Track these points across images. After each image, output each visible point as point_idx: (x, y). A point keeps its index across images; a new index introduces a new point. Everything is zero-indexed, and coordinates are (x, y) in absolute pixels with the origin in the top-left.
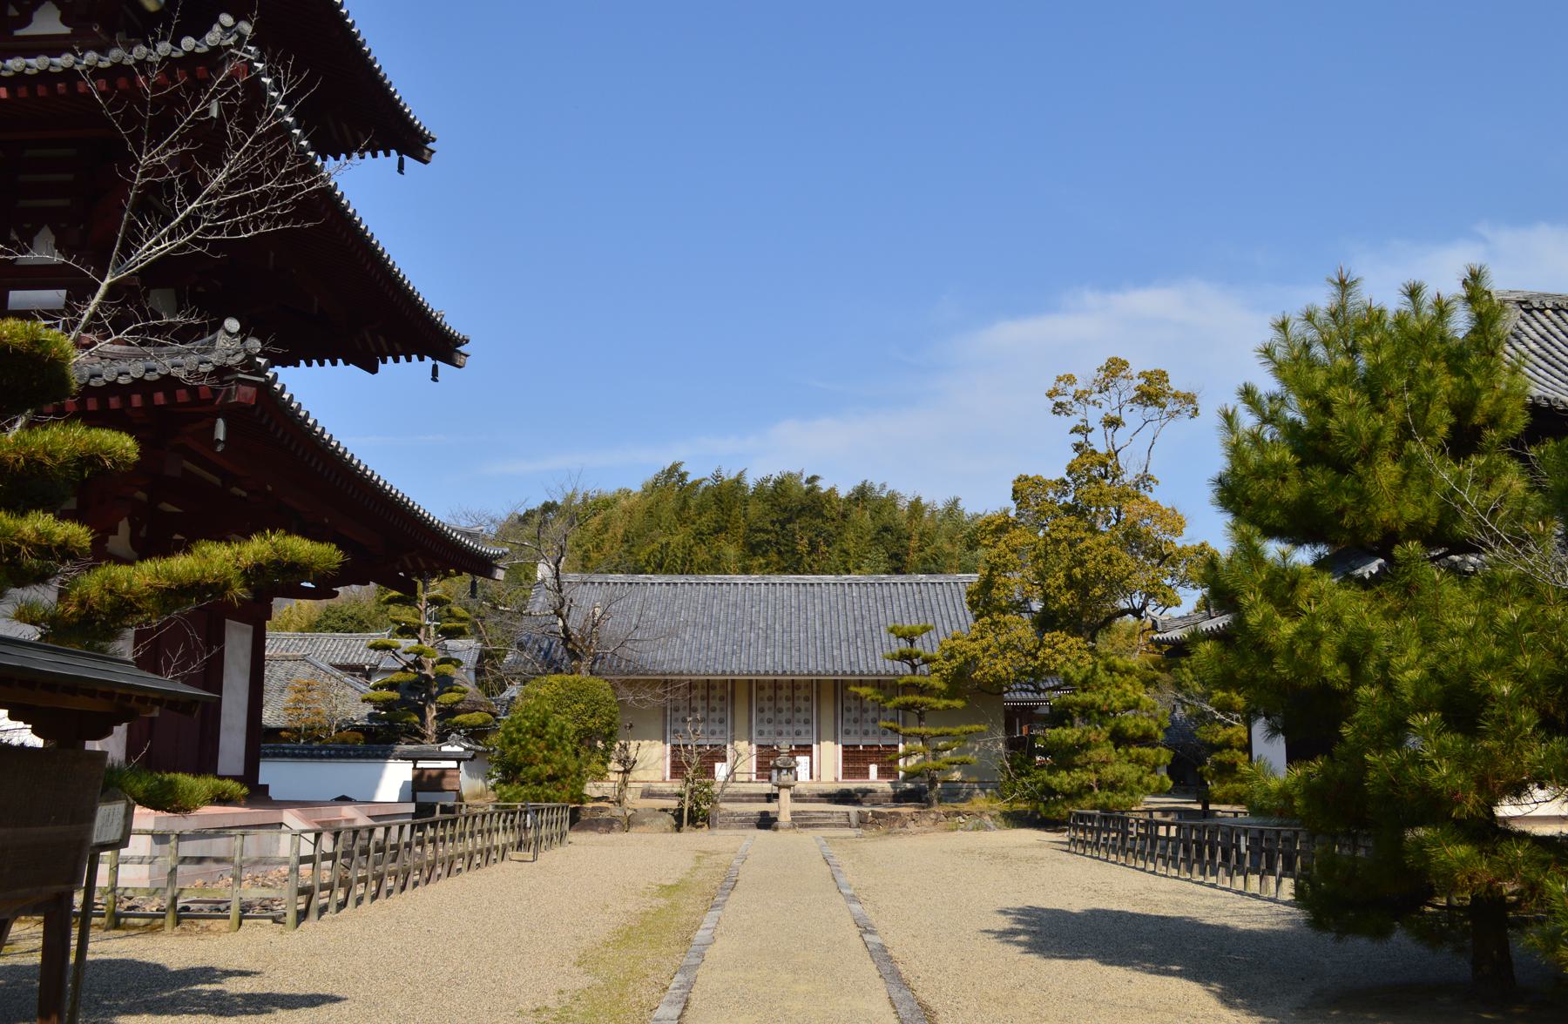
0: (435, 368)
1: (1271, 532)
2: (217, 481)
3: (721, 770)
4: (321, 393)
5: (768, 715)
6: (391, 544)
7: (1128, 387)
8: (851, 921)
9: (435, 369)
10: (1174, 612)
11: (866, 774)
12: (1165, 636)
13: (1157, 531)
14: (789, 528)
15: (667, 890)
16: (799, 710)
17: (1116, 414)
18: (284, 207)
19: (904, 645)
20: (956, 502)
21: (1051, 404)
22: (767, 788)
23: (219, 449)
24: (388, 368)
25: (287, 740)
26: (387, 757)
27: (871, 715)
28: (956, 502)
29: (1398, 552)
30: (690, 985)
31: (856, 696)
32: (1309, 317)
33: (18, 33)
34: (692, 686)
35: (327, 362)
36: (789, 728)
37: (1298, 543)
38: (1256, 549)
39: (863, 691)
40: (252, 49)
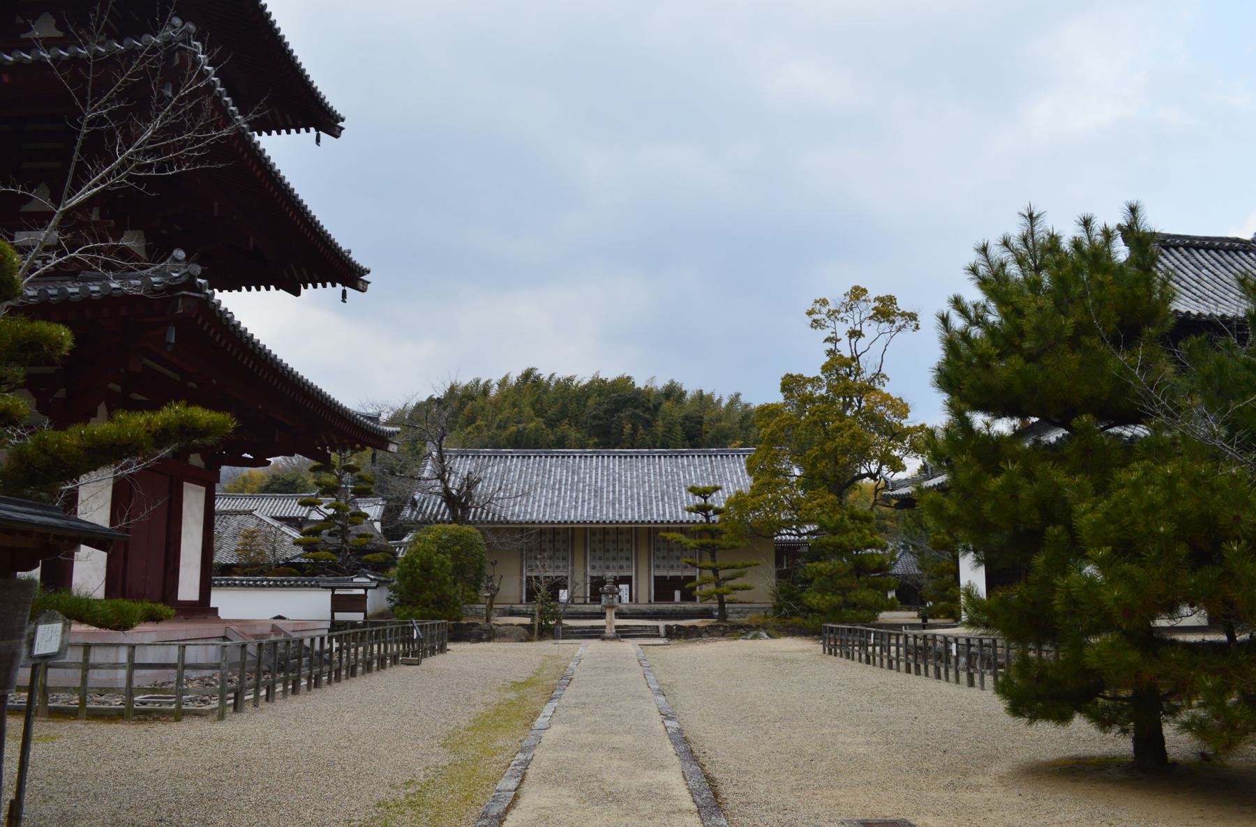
0: (344, 292)
1: (977, 407)
2: (177, 378)
3: (563, 595)
4: (259, 312)
5: (599, 554)
6: (287, 414)
7: (867, 308)
8: (656, 710)
9: (344, 293)
10: (900, 475)
11: (671, 599)
12: (896, 492)
13: (890, 416)
14: (617, 418)
15: (516, 686)
16: (622, 550)
17: (858, 328)
18: (200, 150)
19: (699, 500)
20: (738, 395)
21: (809, 320)
22: (597, 608)
23: (170, 349)
24: (308, 292)
27: (676, 553)
28: (738, 395)
29: (1075, 422)
30: (526, 764)
31: (664, 540)
32: (1006, 243)
33: (24, 36)
34: (542, 532)
35: (263, 288)
36: (614, 564)
37: (998, 416)
38: (967, 419)
39: (670, 536)
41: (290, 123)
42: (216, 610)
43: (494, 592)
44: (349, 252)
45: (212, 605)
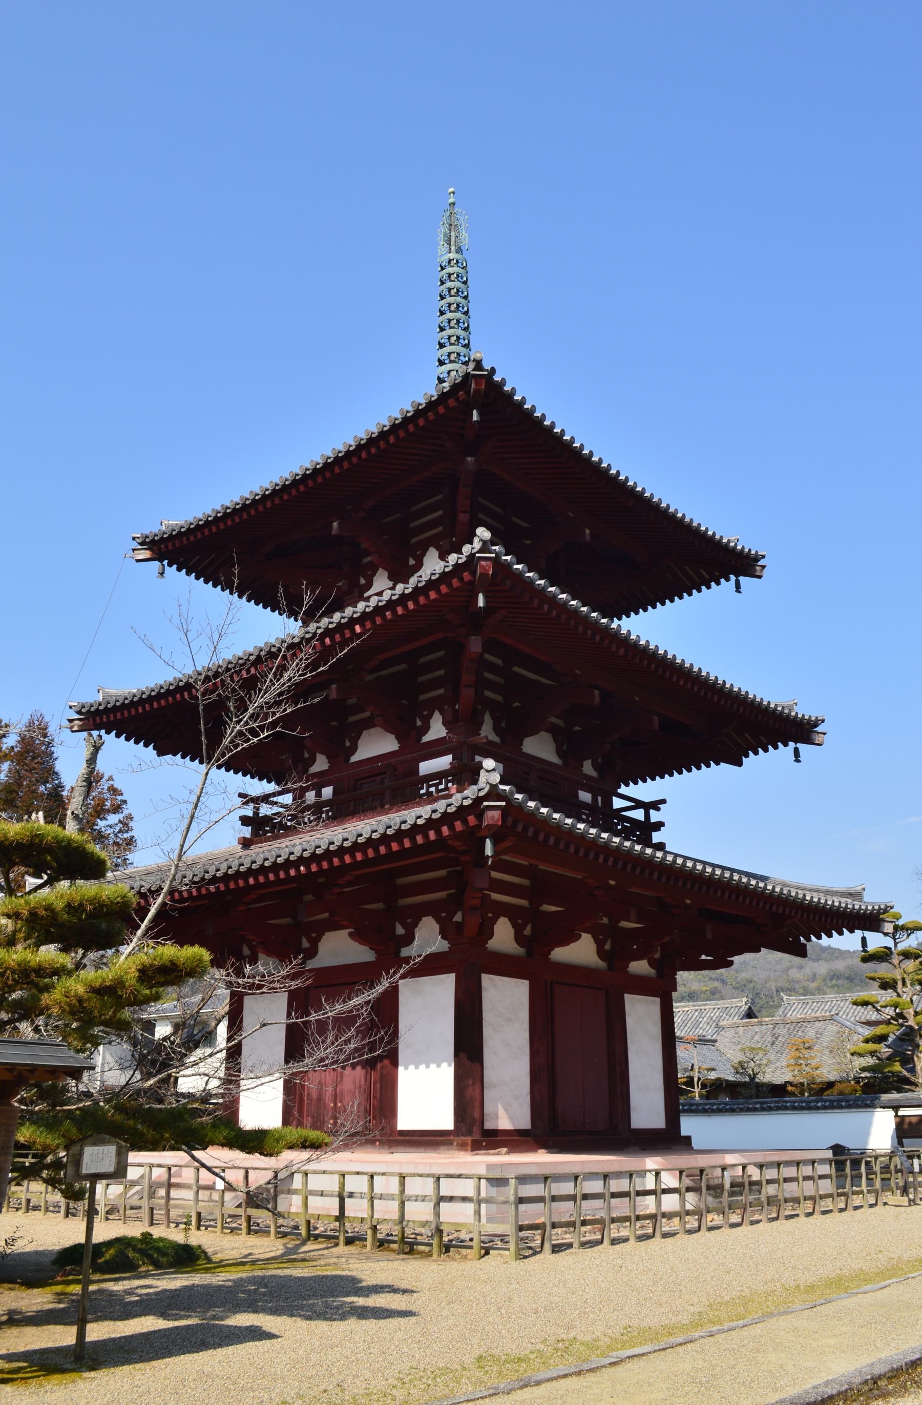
9: (796, 751)
24: (751, 761)
25: (793, 1094)
26: (873, 1106)
42: (688, 1139)
45: (684, 1133)
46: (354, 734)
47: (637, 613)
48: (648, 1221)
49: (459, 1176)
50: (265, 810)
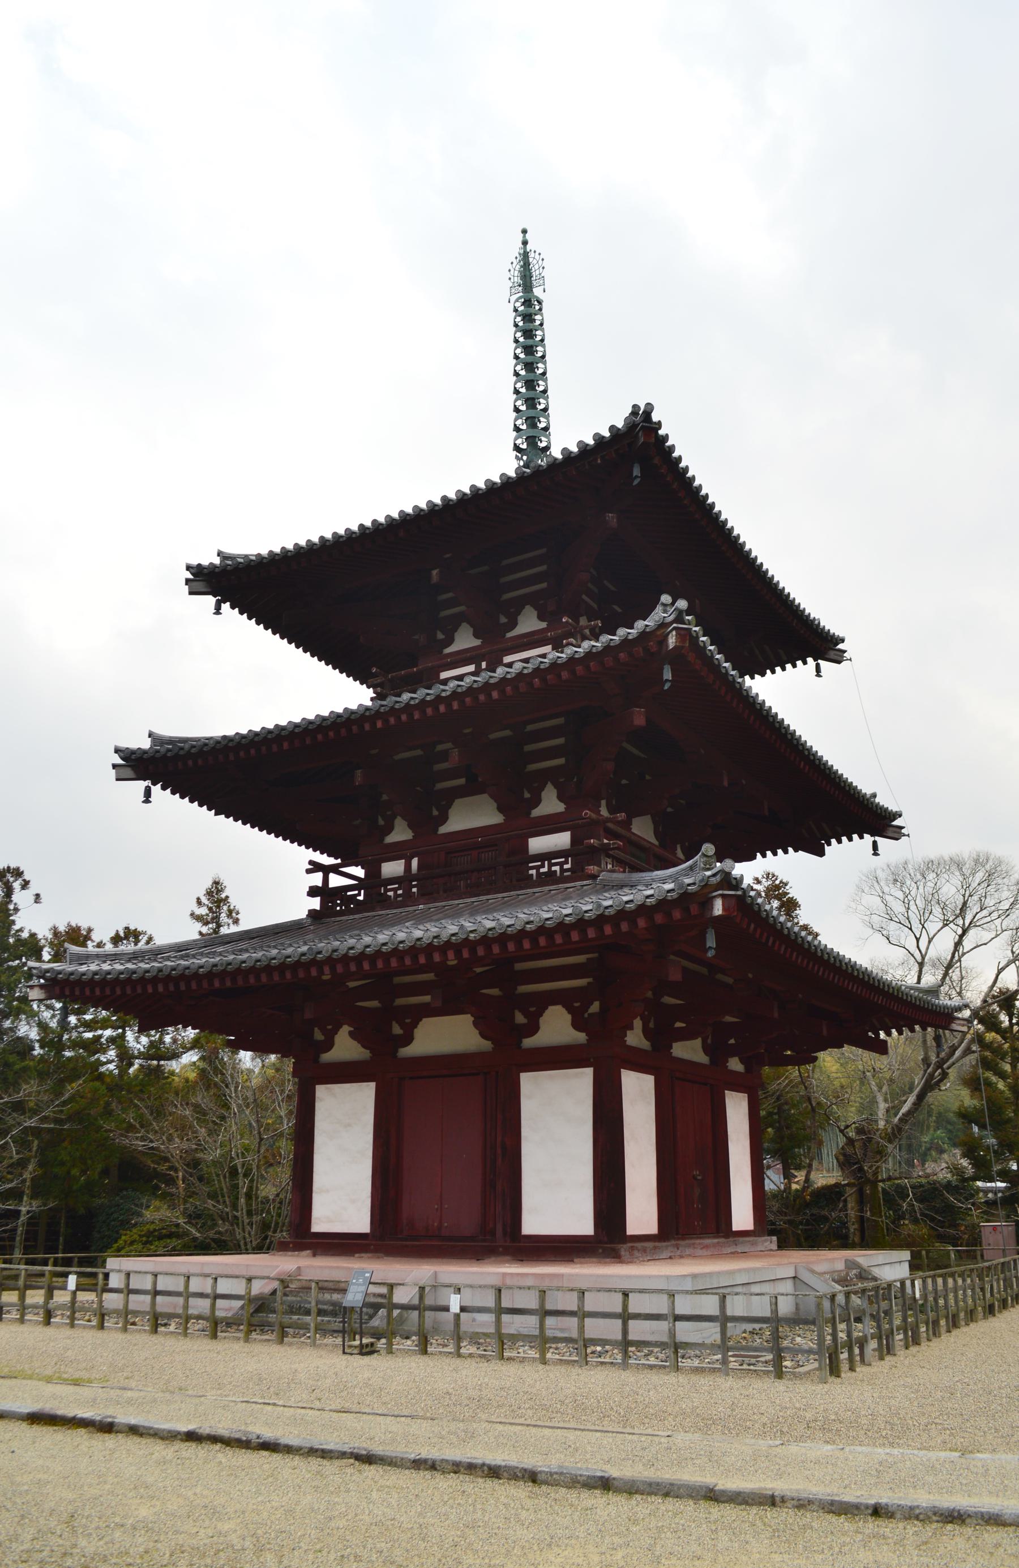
0: (875, 843)
9: (875, 845)
23: (710, 954)
24: (834, 849)
40: (689, 618)
41: (785, 658)
43: (912, 988)
44: (874, 796)
46: (445, 802)
47: (250, 618)
48: (765, 1326)
49: (107, 1428)
50: (336, 881)
